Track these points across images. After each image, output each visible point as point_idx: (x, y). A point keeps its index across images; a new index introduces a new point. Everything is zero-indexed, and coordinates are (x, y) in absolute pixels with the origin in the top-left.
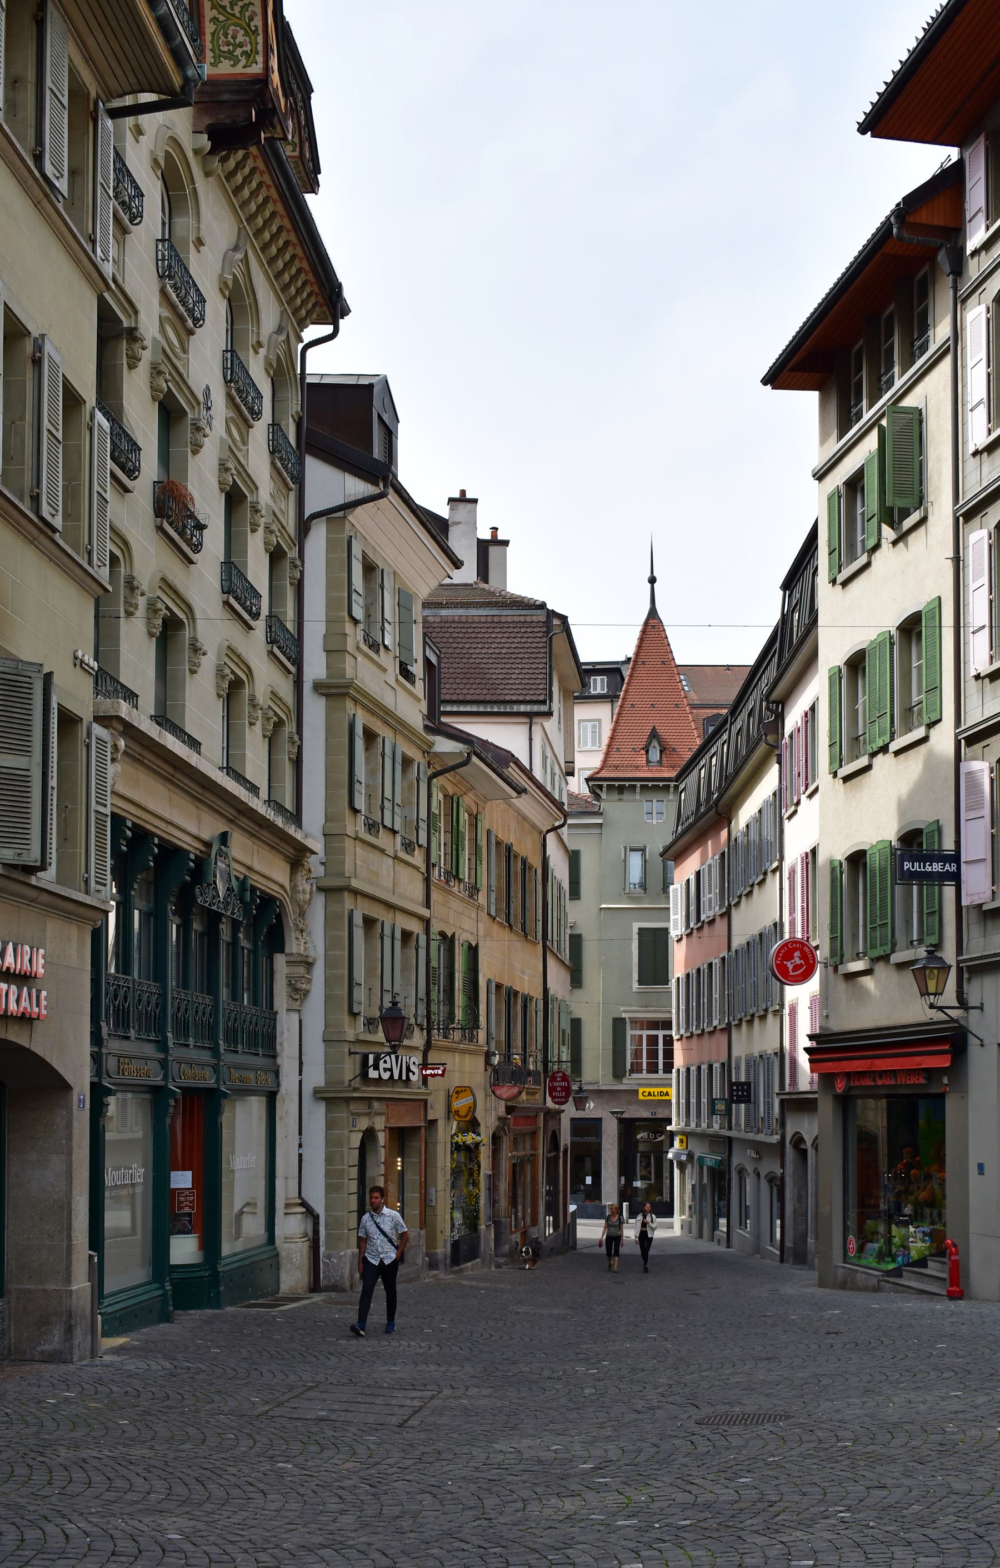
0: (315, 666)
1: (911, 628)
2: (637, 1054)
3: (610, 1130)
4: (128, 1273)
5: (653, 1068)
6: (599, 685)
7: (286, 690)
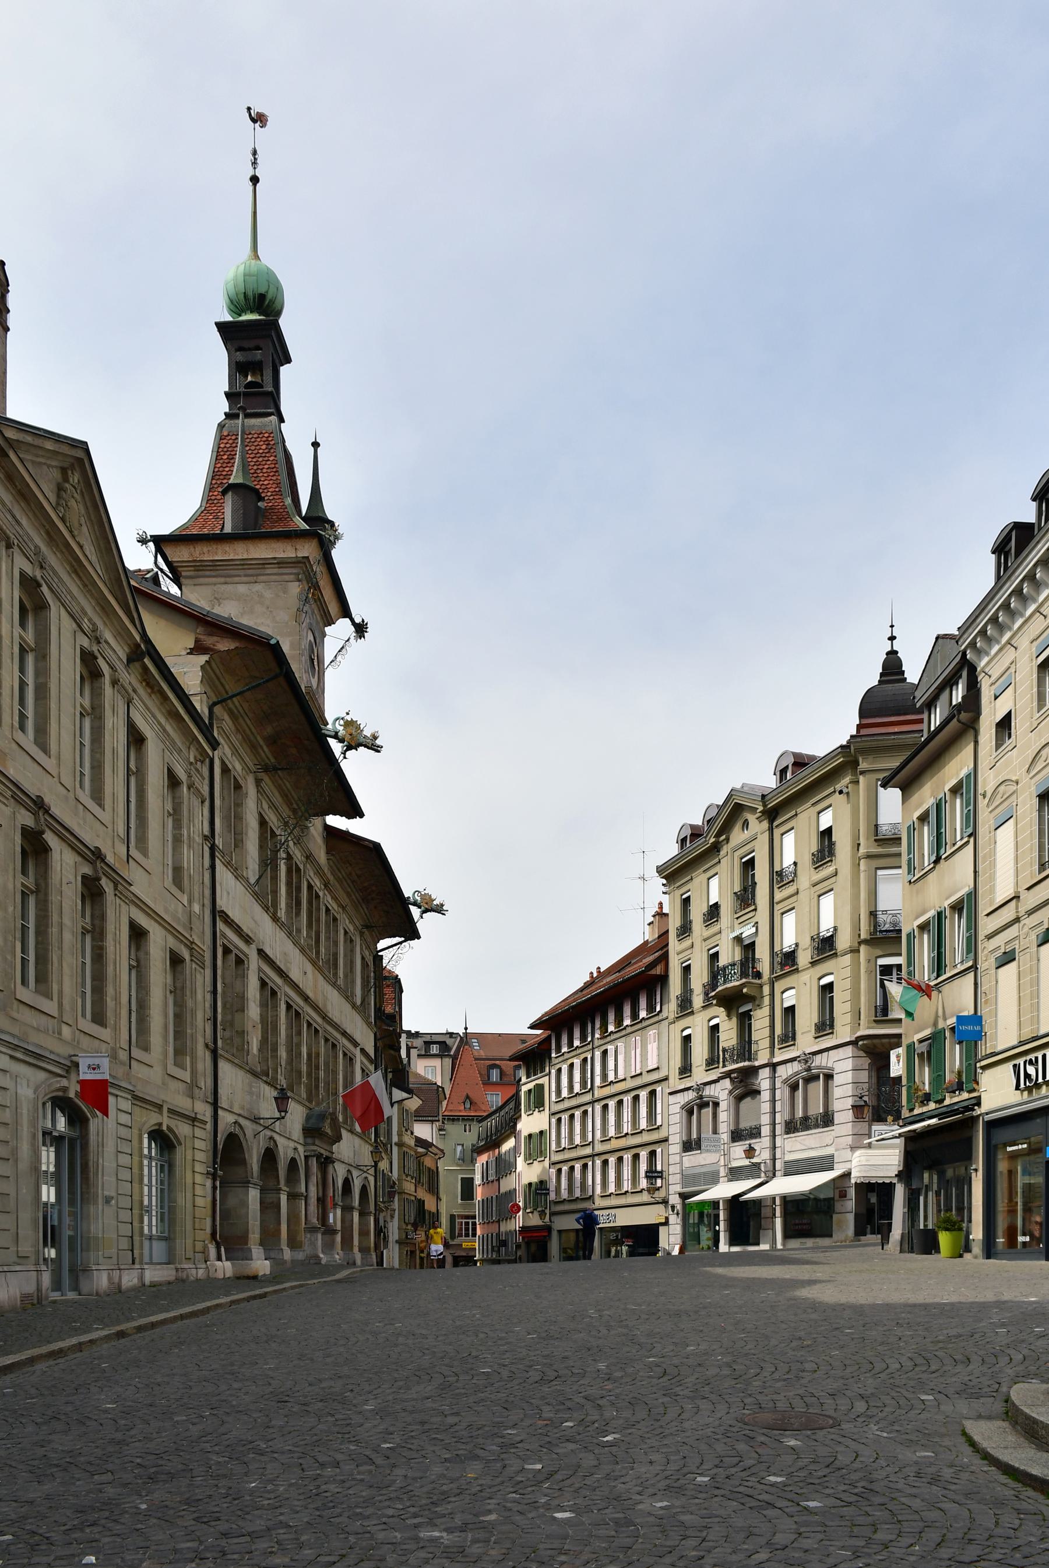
1: (541, 1132)
2: (461, 1229)
5: (467, 1235)
6: (435, 1049)
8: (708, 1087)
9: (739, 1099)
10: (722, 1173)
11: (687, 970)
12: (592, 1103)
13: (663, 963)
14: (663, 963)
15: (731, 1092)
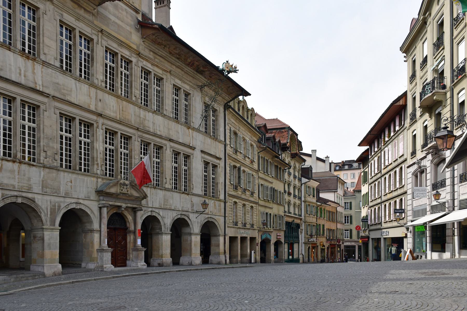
0: (303, 199)
3: (357, 247)
4: (286, 258)
7: (300, 202)
8: (423, 161)
9: (437, 165)
10: (428, 210)
11: (414, 99)
12: (381, 177)
13: (404, 99)
14: (404, 99)
15: (432, 161)
